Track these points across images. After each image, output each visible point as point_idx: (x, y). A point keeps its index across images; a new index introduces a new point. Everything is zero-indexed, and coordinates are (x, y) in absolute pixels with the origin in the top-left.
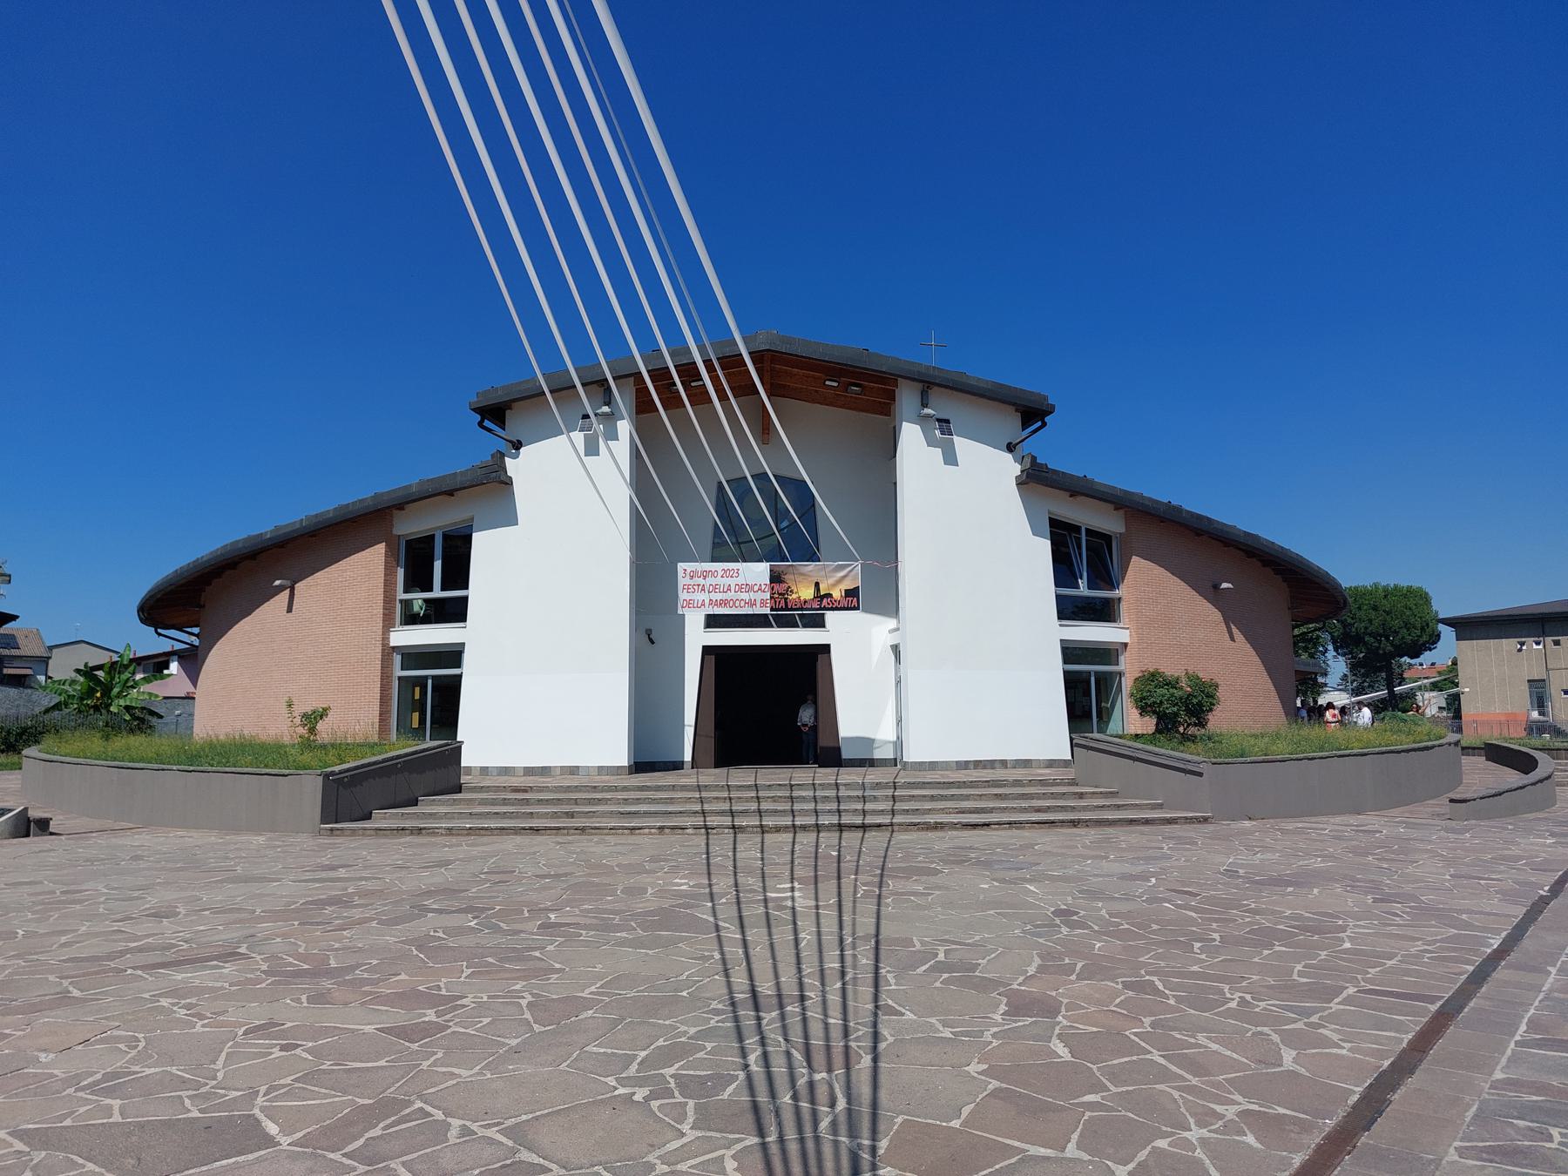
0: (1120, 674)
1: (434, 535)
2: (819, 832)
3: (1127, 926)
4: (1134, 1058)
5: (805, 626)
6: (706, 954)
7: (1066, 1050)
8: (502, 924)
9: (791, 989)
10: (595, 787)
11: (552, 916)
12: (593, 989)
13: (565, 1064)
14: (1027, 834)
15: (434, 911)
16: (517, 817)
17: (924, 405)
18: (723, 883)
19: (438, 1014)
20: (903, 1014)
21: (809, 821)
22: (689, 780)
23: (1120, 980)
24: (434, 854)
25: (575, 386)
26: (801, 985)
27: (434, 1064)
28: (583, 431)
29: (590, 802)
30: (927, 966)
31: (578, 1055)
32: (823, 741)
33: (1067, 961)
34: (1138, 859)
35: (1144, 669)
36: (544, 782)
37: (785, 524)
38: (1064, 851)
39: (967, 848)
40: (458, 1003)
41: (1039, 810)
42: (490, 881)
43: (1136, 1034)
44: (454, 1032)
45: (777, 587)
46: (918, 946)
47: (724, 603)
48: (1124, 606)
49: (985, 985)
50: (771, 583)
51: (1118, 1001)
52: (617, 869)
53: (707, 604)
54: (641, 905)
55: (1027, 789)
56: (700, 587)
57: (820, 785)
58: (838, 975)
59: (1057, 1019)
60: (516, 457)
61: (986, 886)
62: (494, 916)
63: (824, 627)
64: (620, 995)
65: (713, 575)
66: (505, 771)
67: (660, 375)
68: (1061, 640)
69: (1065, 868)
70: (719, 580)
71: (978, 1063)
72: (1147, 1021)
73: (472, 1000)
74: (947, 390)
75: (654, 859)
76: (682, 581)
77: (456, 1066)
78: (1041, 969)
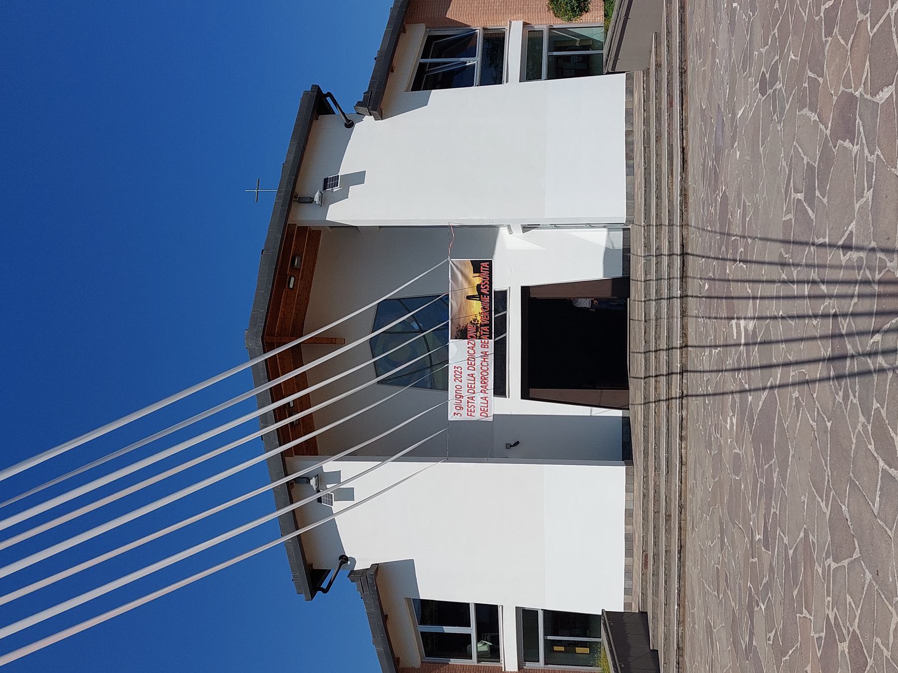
0: (551, 29)
1: (421, 632)
2: (687, 296)
3: (776, 31)
4: (893, 29)
5: (505, 309)
6: (794, 404)
7: (886, 89)
8: (764, 581)
9: (828, 326)
10: (644, 495)
11: (758, 537)
12: (823, 505)
13: (889, 532)
14: (692, 114)
15: (751, 640)
16: (670, 564)
17: (311, 200)
18: (731, 382)
19: (843, 640)
20: (851, 232)
21: (677, 308)
22: (640, 413)
23: (824, 39)
24: (701, 637)
25: (293, 511)
26: (825, 316)
27: (886, 645)
28: (332, 502)
29: (657, 500)
30: (809, 209)
31: (881, 520)
32: (607, 293)
33: (806, 85)
34: (715, 17)
35: (547, 9)
36: (639, 541)
37: (415, 325)
38: (707, 83)
39: (704, 168)
40: (833, 622)
41: (671, 104)
42: (725, 591)
43: (872, 28)
44: (859, 628)
45: (470, 333)
46: (790, 216)
47: (484, 379)
48: (490, 25)
49: (826, 158)
50: (467, 339)
51: (842, 42)
52: (717, 479)
53: (485, 395)
54: (750, 459)
55: (651, 113)
56: (470, 401)
57: (645, 297)
58: (815, 287)
59: (858, 96)
60: (354, 561)
61: (738, 153)
62: (756, 589)
63: (506, 292)
64: (829, 481)
65: (459, 389)
66: (628, 572)
67: (284, 435)
68: (520, 82)
69: (723, 82)
70: (464, 384)
71: (896, 168)
72: (860, 17)
73: (831, 609)
74: (298, 180)
75: (709, 446)
76: (464, 416)
77: (888, 626)
78: (813, 109)
